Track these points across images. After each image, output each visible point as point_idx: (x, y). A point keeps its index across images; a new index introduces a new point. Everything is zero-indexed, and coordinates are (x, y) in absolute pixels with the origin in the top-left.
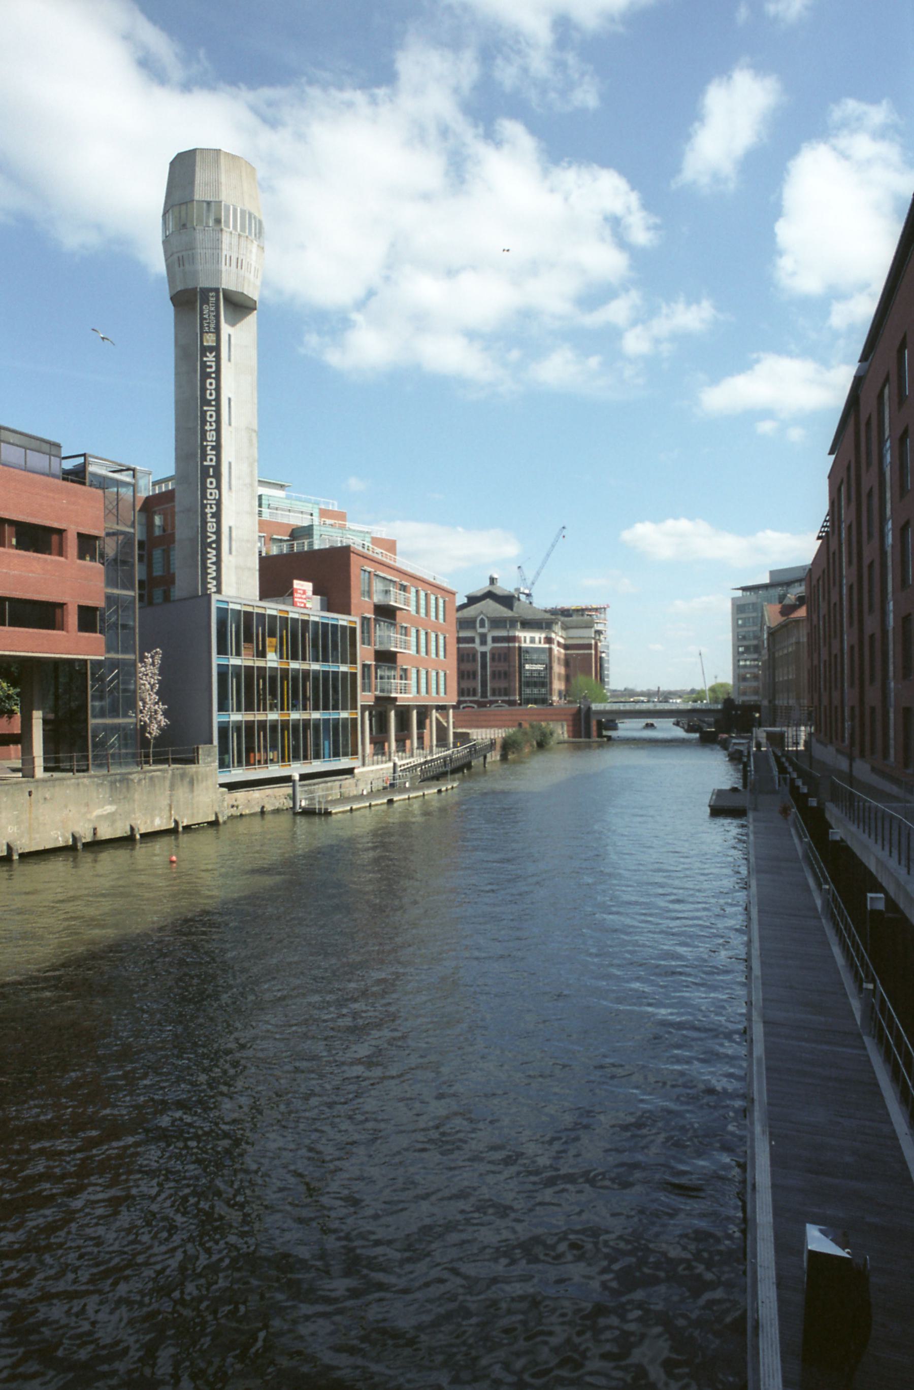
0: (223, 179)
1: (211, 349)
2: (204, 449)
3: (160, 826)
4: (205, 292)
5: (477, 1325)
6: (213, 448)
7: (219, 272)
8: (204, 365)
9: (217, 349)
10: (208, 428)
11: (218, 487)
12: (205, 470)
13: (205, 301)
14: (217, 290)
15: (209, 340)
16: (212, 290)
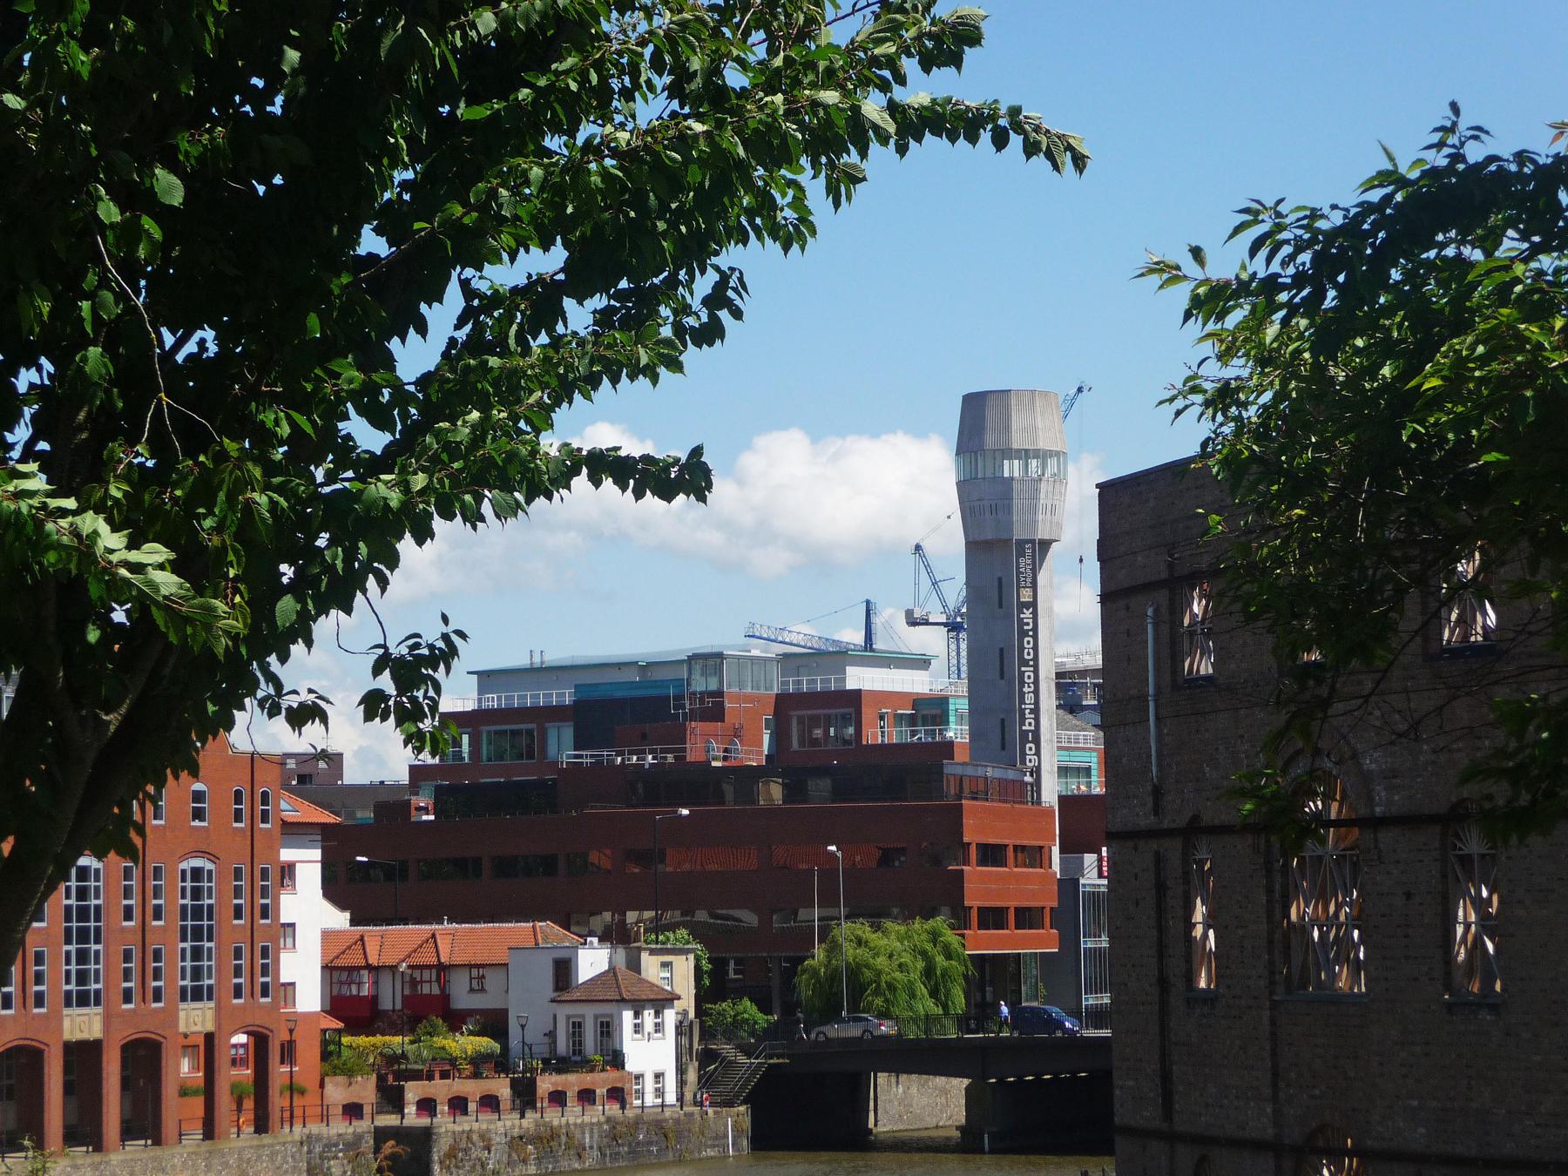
0: (1040, 424)
1: (1027, 605)
2: (1022, 712)
3: (1050, 610)
4: (1021, 544)
5: (1474, 286)
6: (1032, 711)
7: (1035, 522)
8: (1021, 623)
9: (1033, 605)
10: (1026, 689)
11: (1038, 753)
12: (1024, 734)
13: (1021, 553)
14: (1033, 542)
15: (1026, 595)
16: (1028, 541)
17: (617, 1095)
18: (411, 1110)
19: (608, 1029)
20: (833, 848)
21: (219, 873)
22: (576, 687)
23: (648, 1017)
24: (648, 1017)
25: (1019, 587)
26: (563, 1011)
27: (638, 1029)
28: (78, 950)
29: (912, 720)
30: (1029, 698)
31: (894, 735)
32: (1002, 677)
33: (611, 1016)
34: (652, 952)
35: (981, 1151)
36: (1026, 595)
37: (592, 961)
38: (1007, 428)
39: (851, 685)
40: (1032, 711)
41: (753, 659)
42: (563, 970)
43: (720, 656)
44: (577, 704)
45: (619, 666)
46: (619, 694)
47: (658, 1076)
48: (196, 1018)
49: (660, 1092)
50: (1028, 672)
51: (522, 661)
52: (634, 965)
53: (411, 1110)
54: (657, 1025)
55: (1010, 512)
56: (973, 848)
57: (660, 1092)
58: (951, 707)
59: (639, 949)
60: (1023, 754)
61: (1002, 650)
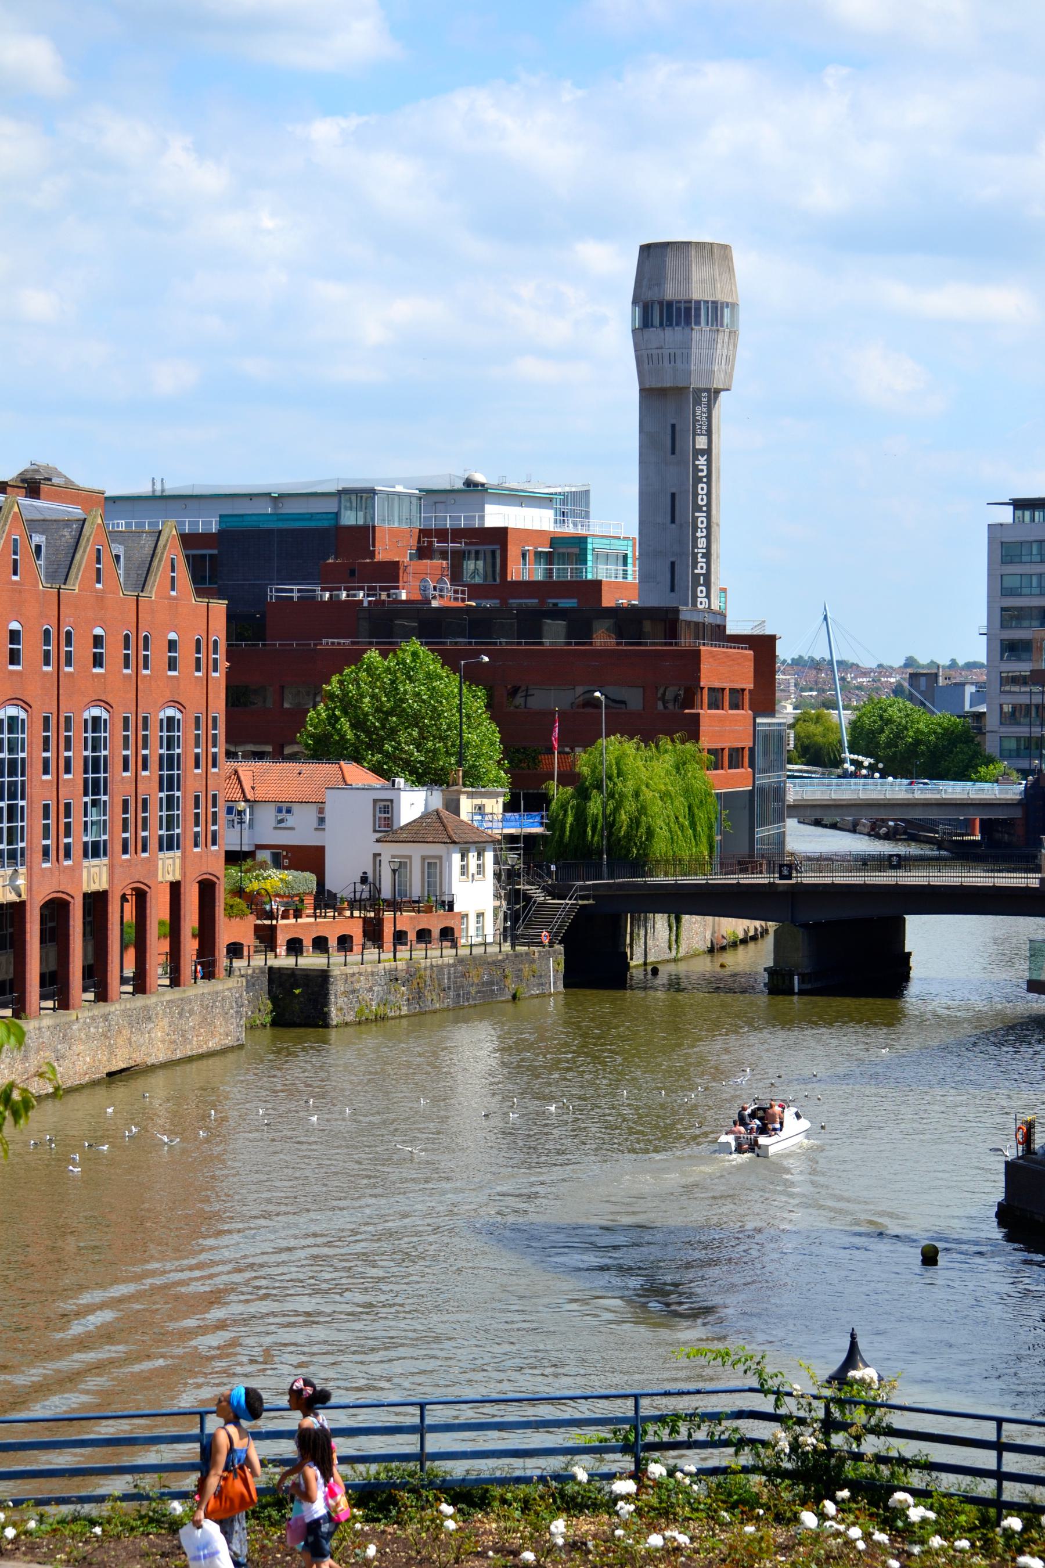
1: (702, 452)
2: (695, 556)
4: (698, 391)
6: (704, 555)
9: (708, 452)
10: (699, 534)
11: (708, 596)
13: (697, 402)
15: (701, 443)
17: (447, 934)
18: (282, 950)
19: (434, 869)
20: (597, 694)
21: (185, 722)
22: (221, 516)
23: (472, 858)
24: (472, 858)
25: (695, 435)
26: (388, 851)
27: (464, 870)
28: (93, 800)
29: (549, 558)
30: (702, 543)
31: (536, 573)
32: (673, 521)
33: (440, 858)
34: (471, 795)
35: (791, 992)
36: (701, 443)
37: (413, 803)
38: (688, 279)
39: (488, 524)
40: (704, 555)
41: (399, 495)
42: (386, 809)
43: (373, 492)
44: (221, 533)
45: (251, 496)
46: (264, 526)
47: (480, 915)
48: (168, 867)
49: (481, 929)
50: (701, 517)
51: (144, 488)
52: (453, 807)
53: (282, 950)
54: (479, 866)
55: (688, 362)
56: (705, 692)
57: (481, 929)
58: (590, 546)
59: (460, 792)
60: (695, 597)
61: (673, 495)
